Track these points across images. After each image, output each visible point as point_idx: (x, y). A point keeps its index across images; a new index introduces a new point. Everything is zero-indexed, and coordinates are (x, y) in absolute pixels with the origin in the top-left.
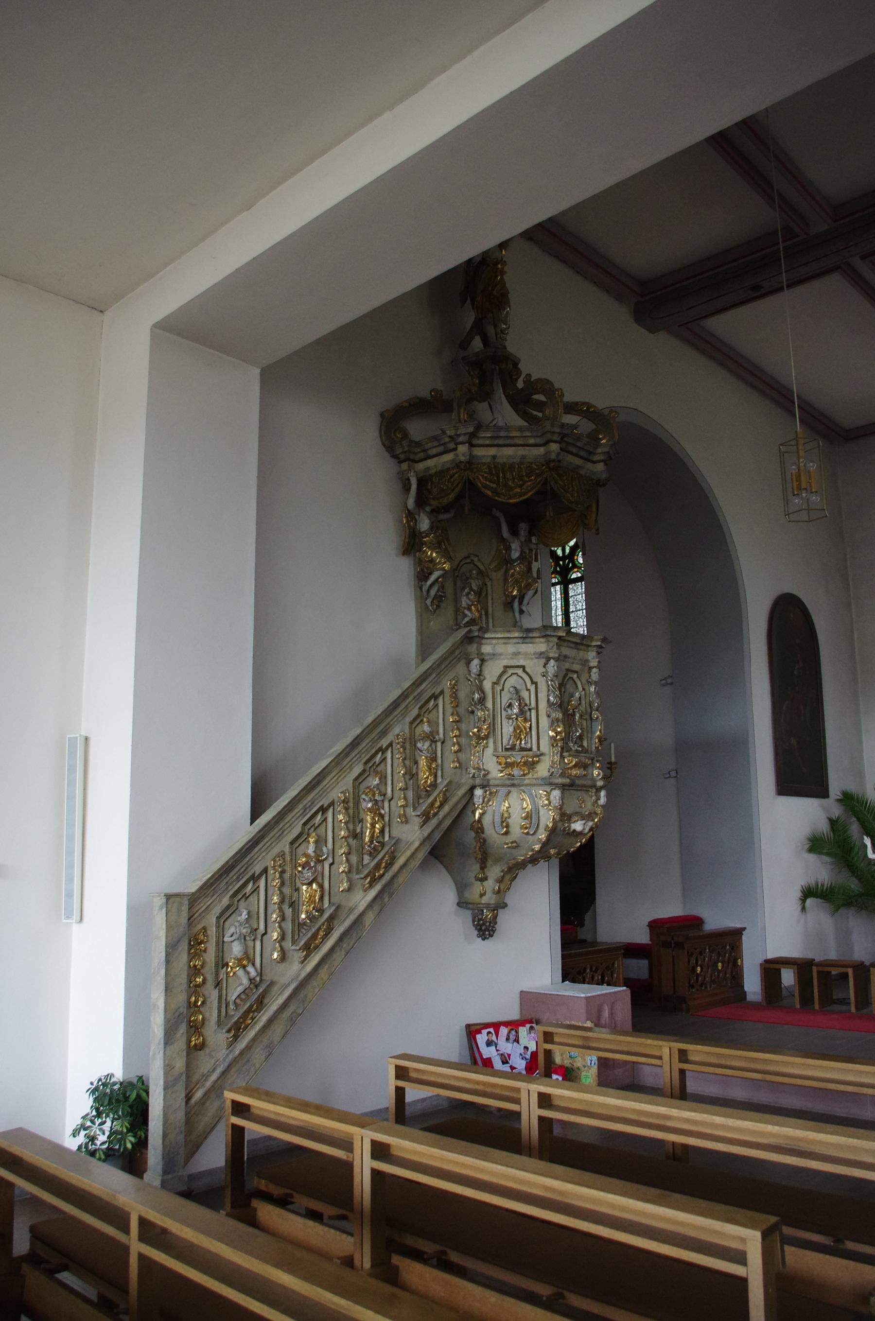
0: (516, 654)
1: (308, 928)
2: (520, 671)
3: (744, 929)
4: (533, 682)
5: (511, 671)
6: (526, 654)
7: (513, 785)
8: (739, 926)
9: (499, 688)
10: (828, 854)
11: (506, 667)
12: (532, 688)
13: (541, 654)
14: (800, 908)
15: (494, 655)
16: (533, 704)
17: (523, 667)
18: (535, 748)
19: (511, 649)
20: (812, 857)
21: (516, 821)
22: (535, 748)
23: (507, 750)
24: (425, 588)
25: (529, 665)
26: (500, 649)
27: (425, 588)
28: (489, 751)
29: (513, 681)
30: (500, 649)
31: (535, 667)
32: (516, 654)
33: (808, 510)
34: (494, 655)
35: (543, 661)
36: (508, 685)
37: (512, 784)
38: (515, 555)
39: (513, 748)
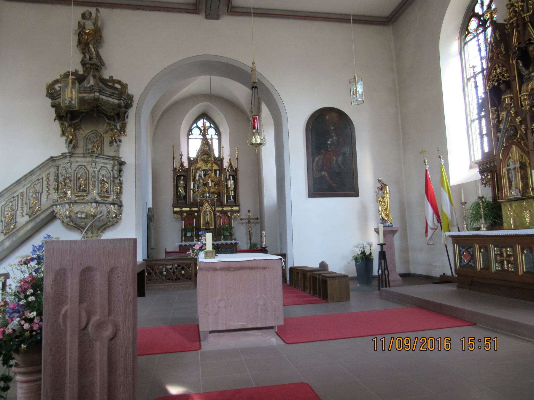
2: (83, 167)
4: (87, 170)
12: (87, 172)
17: (84, 166)
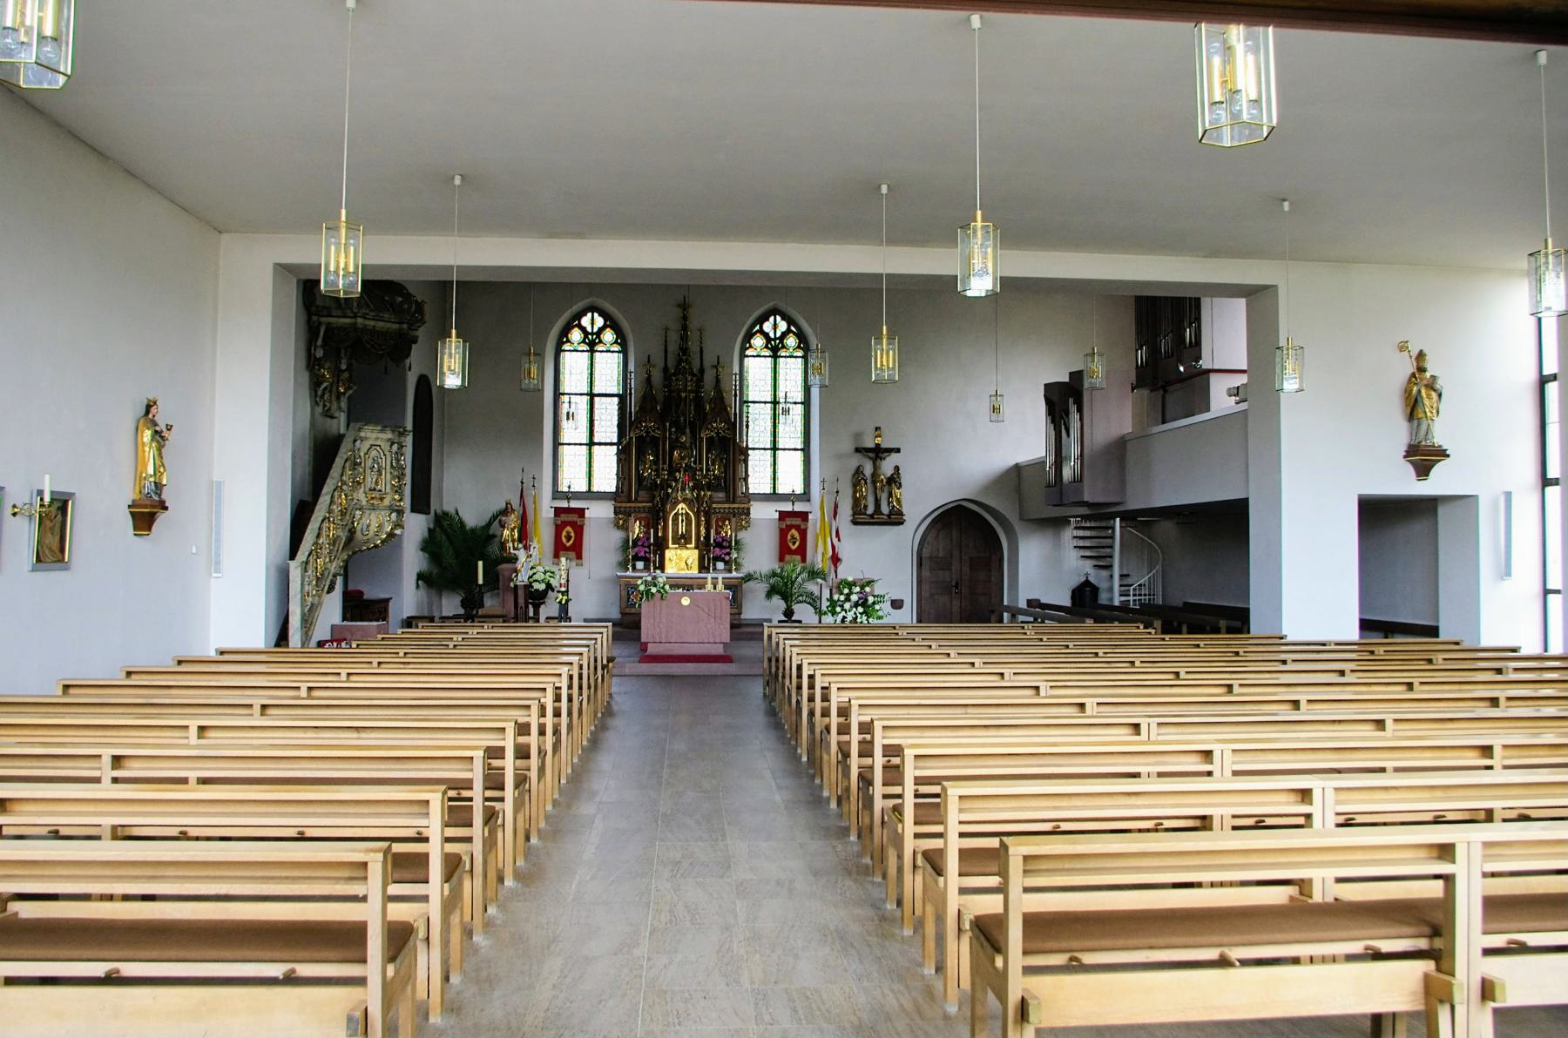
0: (377, 439)
1: (728, 550)
2: (378, 448)
3: (391, 598)
5: (374, 447)
6: (382, 439)
7: (374, 509)
8: (387, 596)
9: (367, 456)
10: (428, 553)
11: (372, 445)
12: (384, 458)
13: (389, 440)
14: (415, 586)
15: (366, 438)
16: (384, 466)
17: (380, 446)
18: (383, 490)
19: (374, 435)
20: (421, 553)
21: (373, 528)
22: (383, 490)
23: (370, 490)
24: (319, 393)
25: (382, 444)
26: (369, 435)
27: (319, 393)
28: (362, 490)
29: (373, 453)
30: (369, 435)
31: (386, 446)
32: (377, 439)
33: (591, 444)
34: (366, 438)
35: (389, 443)
36: (372, 456)
37: (374, 508)
38: (344, 367)
39: (375, 489)
